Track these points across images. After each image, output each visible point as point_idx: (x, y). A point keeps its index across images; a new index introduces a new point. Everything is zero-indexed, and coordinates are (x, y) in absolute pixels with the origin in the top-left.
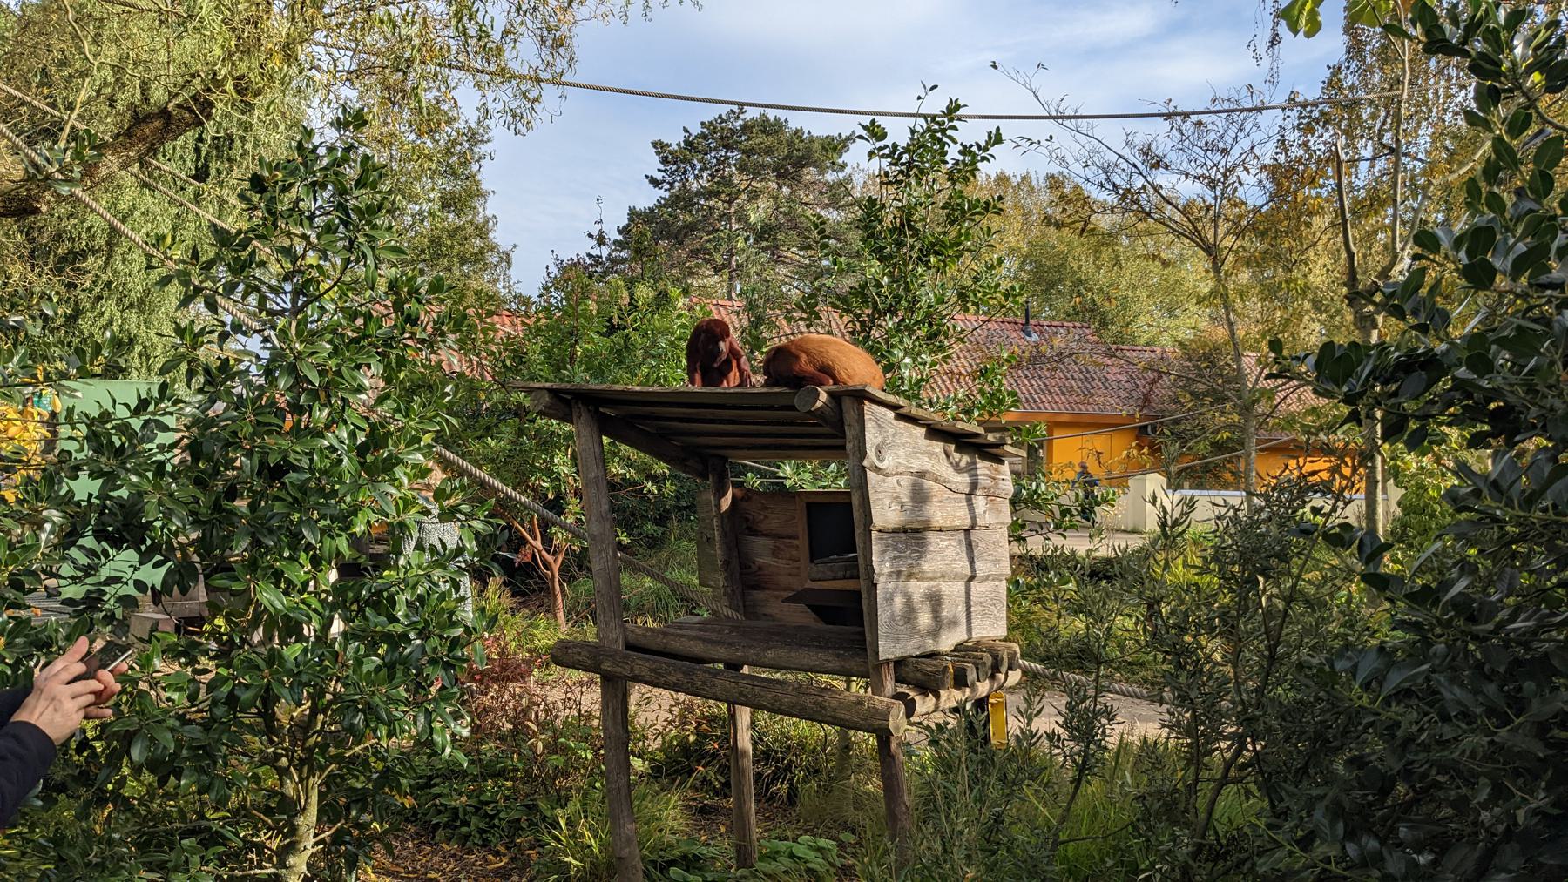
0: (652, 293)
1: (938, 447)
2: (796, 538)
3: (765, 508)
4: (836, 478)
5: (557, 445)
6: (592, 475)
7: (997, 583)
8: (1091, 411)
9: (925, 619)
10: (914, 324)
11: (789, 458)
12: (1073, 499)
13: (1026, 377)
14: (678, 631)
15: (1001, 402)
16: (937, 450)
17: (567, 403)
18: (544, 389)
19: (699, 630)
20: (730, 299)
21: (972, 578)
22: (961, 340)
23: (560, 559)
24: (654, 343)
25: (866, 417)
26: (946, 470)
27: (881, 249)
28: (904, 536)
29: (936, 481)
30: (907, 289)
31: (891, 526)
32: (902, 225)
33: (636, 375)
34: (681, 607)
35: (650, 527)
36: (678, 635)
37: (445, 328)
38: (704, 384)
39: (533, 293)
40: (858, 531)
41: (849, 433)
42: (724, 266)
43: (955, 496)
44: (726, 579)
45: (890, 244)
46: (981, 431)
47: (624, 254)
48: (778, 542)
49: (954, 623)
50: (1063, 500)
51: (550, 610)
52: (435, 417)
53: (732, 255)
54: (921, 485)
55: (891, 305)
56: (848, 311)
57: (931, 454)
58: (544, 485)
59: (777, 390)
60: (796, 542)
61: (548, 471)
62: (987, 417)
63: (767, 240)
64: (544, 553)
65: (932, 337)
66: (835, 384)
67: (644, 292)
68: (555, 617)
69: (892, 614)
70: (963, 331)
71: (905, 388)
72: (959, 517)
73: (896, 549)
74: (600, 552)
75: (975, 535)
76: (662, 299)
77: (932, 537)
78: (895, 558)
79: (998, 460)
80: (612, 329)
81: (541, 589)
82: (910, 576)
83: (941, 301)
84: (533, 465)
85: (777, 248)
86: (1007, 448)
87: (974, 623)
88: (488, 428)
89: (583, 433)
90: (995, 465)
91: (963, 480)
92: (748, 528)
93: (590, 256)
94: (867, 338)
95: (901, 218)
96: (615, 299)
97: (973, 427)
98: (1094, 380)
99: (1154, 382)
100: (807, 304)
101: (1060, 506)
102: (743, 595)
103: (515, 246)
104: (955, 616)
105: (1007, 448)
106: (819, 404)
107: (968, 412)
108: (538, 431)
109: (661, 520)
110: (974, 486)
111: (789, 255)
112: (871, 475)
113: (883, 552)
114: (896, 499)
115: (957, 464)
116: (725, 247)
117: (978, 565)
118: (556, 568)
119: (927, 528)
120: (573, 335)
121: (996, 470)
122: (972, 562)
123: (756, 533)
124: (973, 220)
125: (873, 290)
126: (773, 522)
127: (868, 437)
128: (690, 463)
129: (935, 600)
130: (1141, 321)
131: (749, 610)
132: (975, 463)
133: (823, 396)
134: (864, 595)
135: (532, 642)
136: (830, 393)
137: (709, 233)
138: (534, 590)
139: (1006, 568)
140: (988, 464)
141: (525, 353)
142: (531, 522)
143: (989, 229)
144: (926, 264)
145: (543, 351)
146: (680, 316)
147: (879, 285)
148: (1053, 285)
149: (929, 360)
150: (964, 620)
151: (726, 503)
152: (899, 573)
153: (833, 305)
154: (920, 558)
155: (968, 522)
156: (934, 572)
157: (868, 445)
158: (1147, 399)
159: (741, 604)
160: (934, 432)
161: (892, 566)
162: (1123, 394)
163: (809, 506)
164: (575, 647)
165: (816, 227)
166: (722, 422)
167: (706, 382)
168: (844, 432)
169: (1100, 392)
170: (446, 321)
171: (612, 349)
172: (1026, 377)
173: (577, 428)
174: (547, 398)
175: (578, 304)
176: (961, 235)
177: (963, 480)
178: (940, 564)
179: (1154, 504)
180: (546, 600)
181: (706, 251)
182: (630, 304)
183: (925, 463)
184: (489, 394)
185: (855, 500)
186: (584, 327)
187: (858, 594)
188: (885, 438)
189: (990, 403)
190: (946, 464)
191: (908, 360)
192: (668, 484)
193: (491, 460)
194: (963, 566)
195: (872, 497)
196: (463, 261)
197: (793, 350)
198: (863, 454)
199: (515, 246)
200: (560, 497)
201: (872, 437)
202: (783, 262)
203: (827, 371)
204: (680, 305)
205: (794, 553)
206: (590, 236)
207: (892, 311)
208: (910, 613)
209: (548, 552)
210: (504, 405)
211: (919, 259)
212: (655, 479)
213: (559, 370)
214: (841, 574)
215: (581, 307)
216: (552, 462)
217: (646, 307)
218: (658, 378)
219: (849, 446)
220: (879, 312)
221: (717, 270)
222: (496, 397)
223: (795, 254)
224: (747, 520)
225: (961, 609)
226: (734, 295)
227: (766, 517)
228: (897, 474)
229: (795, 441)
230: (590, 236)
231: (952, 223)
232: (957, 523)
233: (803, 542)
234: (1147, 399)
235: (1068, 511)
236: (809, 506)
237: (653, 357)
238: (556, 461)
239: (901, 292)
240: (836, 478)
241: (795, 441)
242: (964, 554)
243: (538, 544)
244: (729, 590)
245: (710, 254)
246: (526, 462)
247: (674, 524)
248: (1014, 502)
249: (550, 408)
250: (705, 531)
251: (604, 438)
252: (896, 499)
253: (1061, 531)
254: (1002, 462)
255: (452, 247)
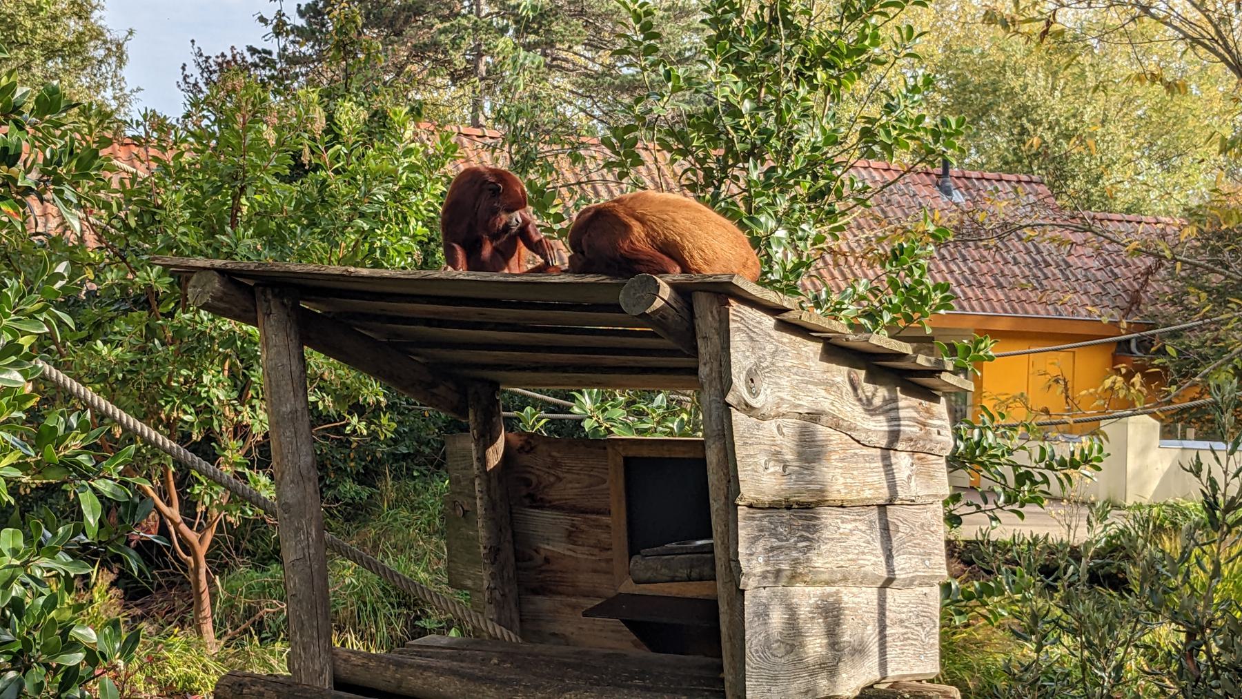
0: (364, 115)
1: (840, 373)
2: (607, 512)
3: (556, 464)
4: (664, 418)
5: (206, 353)
6: (287, 408)
7: (926, 590)
8: (1043, 314)
9: (815, 645)
10: (791, 177)
11: (591, 385)
12: (1036, 455)
13: (943, 258)
14: (418, 660)
15: (923, 299)
16: (839, 379)
17: (250, 292)
18: (213, 269)
19: (451, 657)
20: (478, 126)
21: (889, 582)
22: (862, 202)
23: (209, 536)
24: (368, 193)
25: (732, 325)
26: (852, 412)
27: (739, 57)
28: (786, 515)
29: (837, 427)
30: (780, 121)
31: (767, 499)
32: (774, 20)
33: (337, 245)
34: (398, 616)
35: (349, 488)
36: (419, 666)
37: (62, 171)
38: (470, 268)
39: (174, 107)
40: (715, 506)
41: (703, 349)
42: (467, 73)
43: (865, 451)
44: (493, 576)
45: (753, 49)
46: (907, 348)
47: (307, 49)
48: (578, 520)
49: (859, 651)
50: (1020, 458)
51: (187, 619)
52: (40, 311)
53: (480, 55)
54: (813, 434)
55: (754, 145)
56: (685, 153)
57: (829, 386)
58: (186, 418)
59: (589, 279)
60: (605, 519)
61: (191, 396)
62: (902, 324)
63: (536, 32)
64: (183, 527)
65: (817, 196)
66: (683, 271)
67: (350, 114)
68: (200, 633)
69: (767, 638)
70: (865, 188)
71: (776, 277)
72: (872, 486)
73: (774, 534)
74: (298, 530)
75: (893, 513)
76: (379, 124)
77: (829, 517)
78: (772, 549)
79: (930, 394)
80: (299, 170)
81: (172, 585)
82: (794, 578)
83: (832, 140)
84: (168, 387)
85: (551, 45)
86: (946, 377)
87: (891, 653)
88: (98, 325)
89: (274, 340)
90: (926, 404)
91: (878, 427)
92: (530, 496)
93: (252, 50)
94: (715, 196)
95: (772, 8)
96: (304, 124)
97: (881, 340)
98: (1048, 265)
99: (1149, 272)
100: (622, 141)
101: (1016, 467)
102: (519, 604)
103: (131, 33)
104: (861, 643)
105: (946, 377)
106: (658, 303)
107: (873, 315)
108: (178, 332)
109: (367, 477)
110: (894, 436)
111: (570, 56)
112: (738, 417)
113: (754, 540)
114: (776, 456)
115: (869, 401)
116: (468, 42)
117: (899, 561)
118: (202, 551)
119: (820, 503)
120: (238, 181)
121: (927, 411)
122: (889, 557)
123: (538, 502)
124: (885, 14)
125: (727, 120)
126: (569, 488)
127: (735, 356)
128: (441, 390)
129: (831, 614)
130: (1116, 174)
131: (528, 625)
132: (895, 400)
133: (666, 292)
134: (723, 607)
135: (162, 670)
136: (674, 286)
137: (444, 19)
138: (160, 586)
139: (939, 566)
140: (915, 401)
141: (160, 207)
142: (164, 481)
143: (910, 29)
144: (810, 80)
145: (190, 203)
146: (408, 152)
147: (735, 112)
148: (985, 110)
149: (814, 232)
150: (875, 649)
151: (495, 455)
152: (778, 573)
153: (665, 146)
154: (809, 548)
155: (885, 494)
156: (833, 572)
157: (734, 371)
158: (1135, 300)
159: (515, 616)
160: (835, 351)
161: (767, 562)
162: (1093, 289)
163: (631, 465)
164: (253, 683)
165: (638, 18)
166: (499, 326)
167: (475, 263)
168: (696, 348)
169: (1057, 285)
170: (65, 160)
171: (299, 203)
172: (943, 258)
173: (264, 333)
174: (216, 284)
175: (246, 129)
176: (865, 37)
177: (878, 427)
178: (842, 560)
179: (1197, 474)
180: (178, 602)
181: (435, 45)
182: (327, 131)
183: (820, 399)
184: (98, 272)
185: (712, 456)
186: (255, 167)
187: (712, 606)
188: (761, 359)
189: (907, 302)
190: (852, 399)
191: (782, 233)
192: (384, 420)
193: (97, 377)
194: (874, 563)
195: (740, 452)
196: (50, 53)
197: (622, 214)
198: (726, 383)
199: (131, 33)
200: (210, 437)
201: (741, 357)
202: (560, 68)
203: (673, 252)
204: (408, 134)
205: (604, 536)
206: (262, 20)
207: (755, 153)
208: (793, 635)
209: (191, 526)
210: (124, 289)
211: (799, 73)
212: (359, 409)
213: (212, 233)
214: (683, 573)
215: (251, 135)
216: (199, 381)
217: (354, 138)
218: (372, 250)
219: (703, 371)
220: (736, 157)
221: (455, 78)
222: (111, 277)
223: (581, 55)
224: (528, 483)
225: (872, 632)
226: (482, 120)
227: (559, 479)
228: (778, 416)
229: (610, 360)
230: (262, 20)
231: (852, 18)
232: (867, 494)
233: (618, 519)
234: (1135, 300)
235: (1028, 475)
236: (631, 465)
237: (362, 215)
238: (206, 379)
239: (771, 124)
240: (664, 418)
241: (610, 360)
242: (878, 544)
243: (174, 512)
244: (497, 594)
245: (445, 52)
246: (158, 380)
247: (388, 485)
248: (955, 462)
249: (221, 299)
250: (460, 499)
251: (305, 347)
252: (776, 456)
253: (1016, 507)
254: (935, 399)
255: (33, 32)
